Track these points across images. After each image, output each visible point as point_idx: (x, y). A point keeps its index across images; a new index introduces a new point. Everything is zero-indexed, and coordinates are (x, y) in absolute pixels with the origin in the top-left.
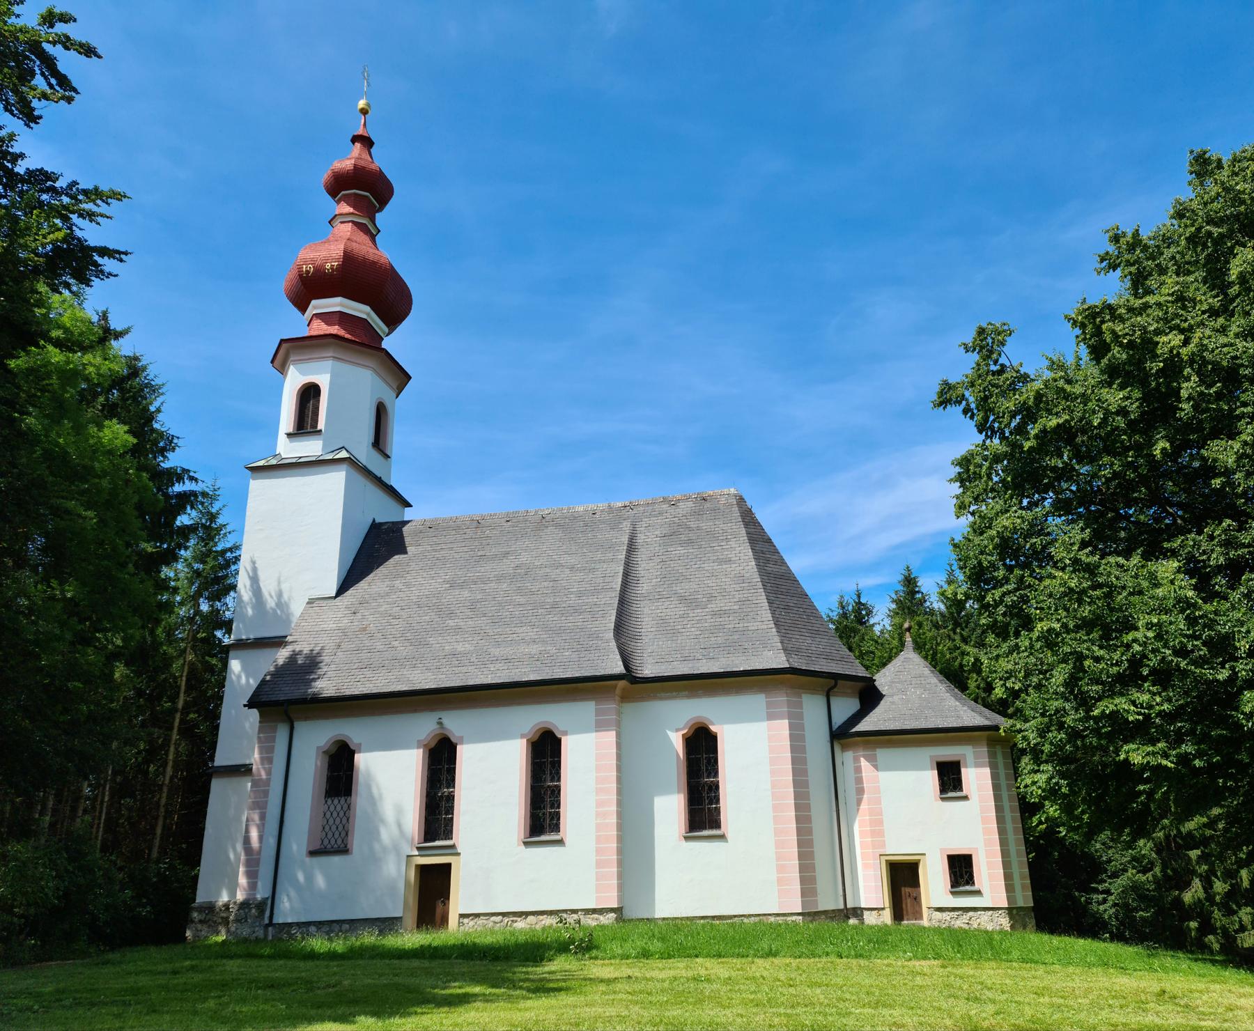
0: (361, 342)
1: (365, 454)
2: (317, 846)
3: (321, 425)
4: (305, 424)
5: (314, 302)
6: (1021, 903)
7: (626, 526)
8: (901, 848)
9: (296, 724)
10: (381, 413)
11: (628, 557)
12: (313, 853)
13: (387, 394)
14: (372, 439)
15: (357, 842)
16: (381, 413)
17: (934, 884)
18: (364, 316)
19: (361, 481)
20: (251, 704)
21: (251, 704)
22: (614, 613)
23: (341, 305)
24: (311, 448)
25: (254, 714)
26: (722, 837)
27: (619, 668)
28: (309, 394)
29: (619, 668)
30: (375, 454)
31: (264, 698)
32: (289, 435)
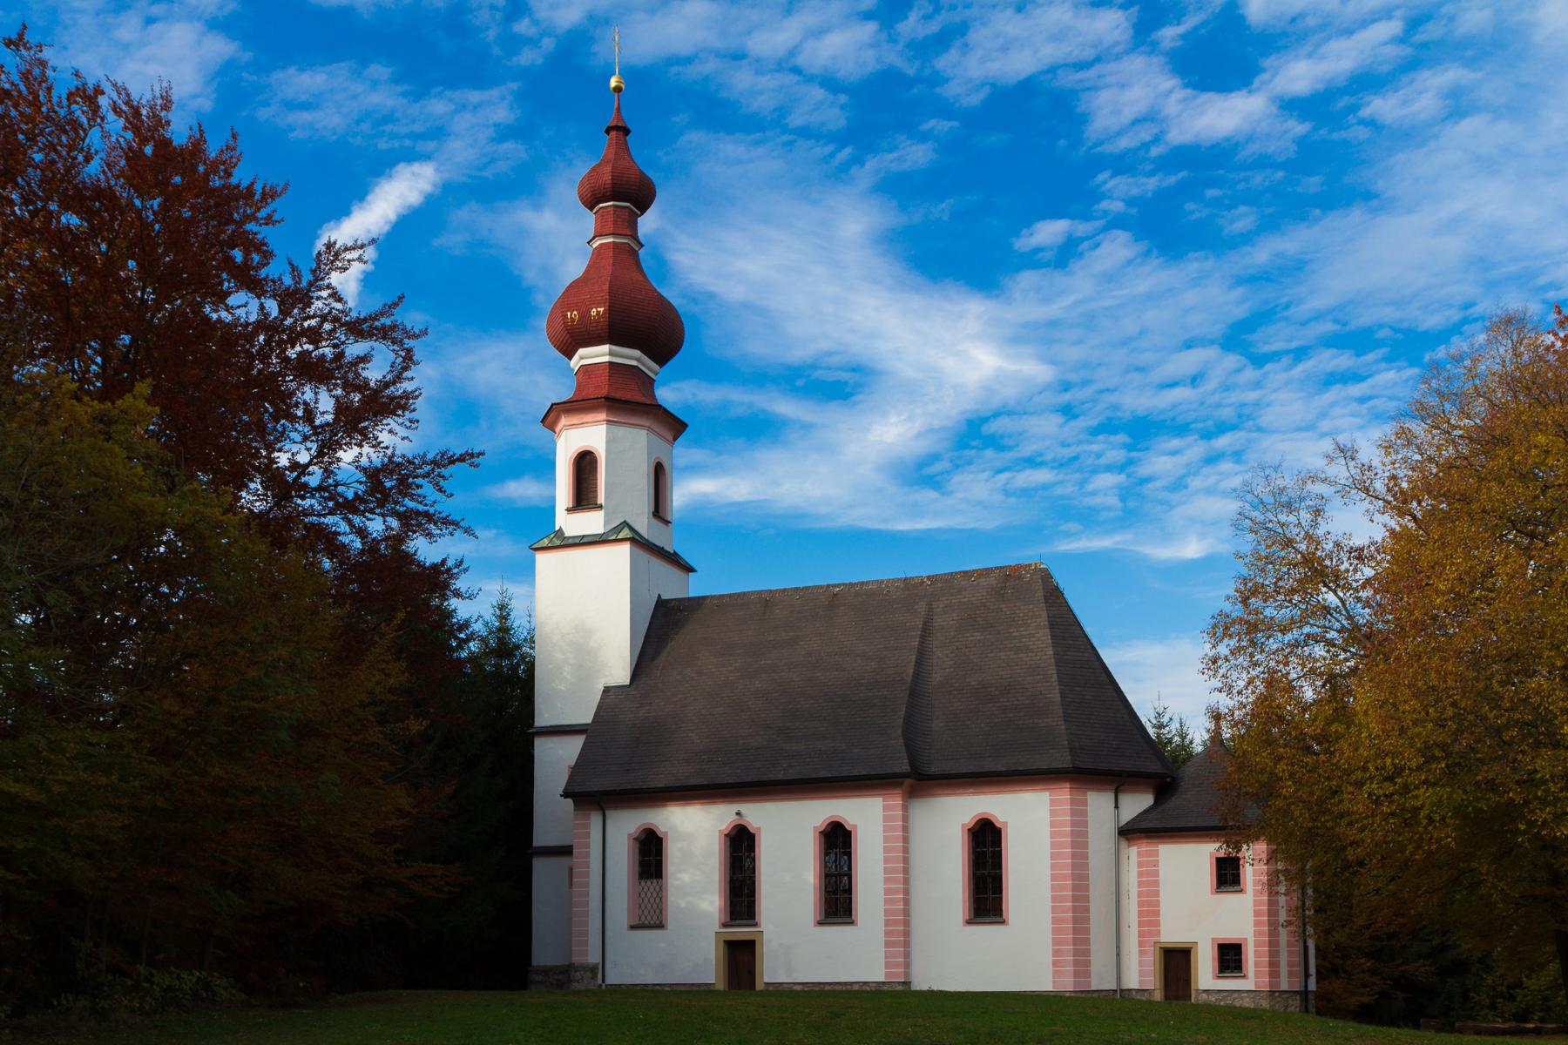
0: (624, 398)
1: (644, 524)
2: (637, 922)
3: (601, 499)
4: (583, 498)
5: (582, 351)
6: (1284, 986)
7: (922, 607)
8: (1173, 934)
9: (608, 813)
10: (659, 471)
11: (923, 642)
12: (633, 927)
13: (662, 450)
14: (652, 509)
15: (671, 917)
16: (659, 471)
17: (1205, 976)
18: (634, 363)
19: (645, 556)
20: (566, 795)
21: (566, 795)
22: (903, 707)
23: (638, 360)
24: (591, 522)
25: (570, 801)
26: (1003, 922)
27: (906, 768)
28: (585, 464)
29: (906, 768)
30: (657, 523)
31: (577, 789)
32: (568, 510)
